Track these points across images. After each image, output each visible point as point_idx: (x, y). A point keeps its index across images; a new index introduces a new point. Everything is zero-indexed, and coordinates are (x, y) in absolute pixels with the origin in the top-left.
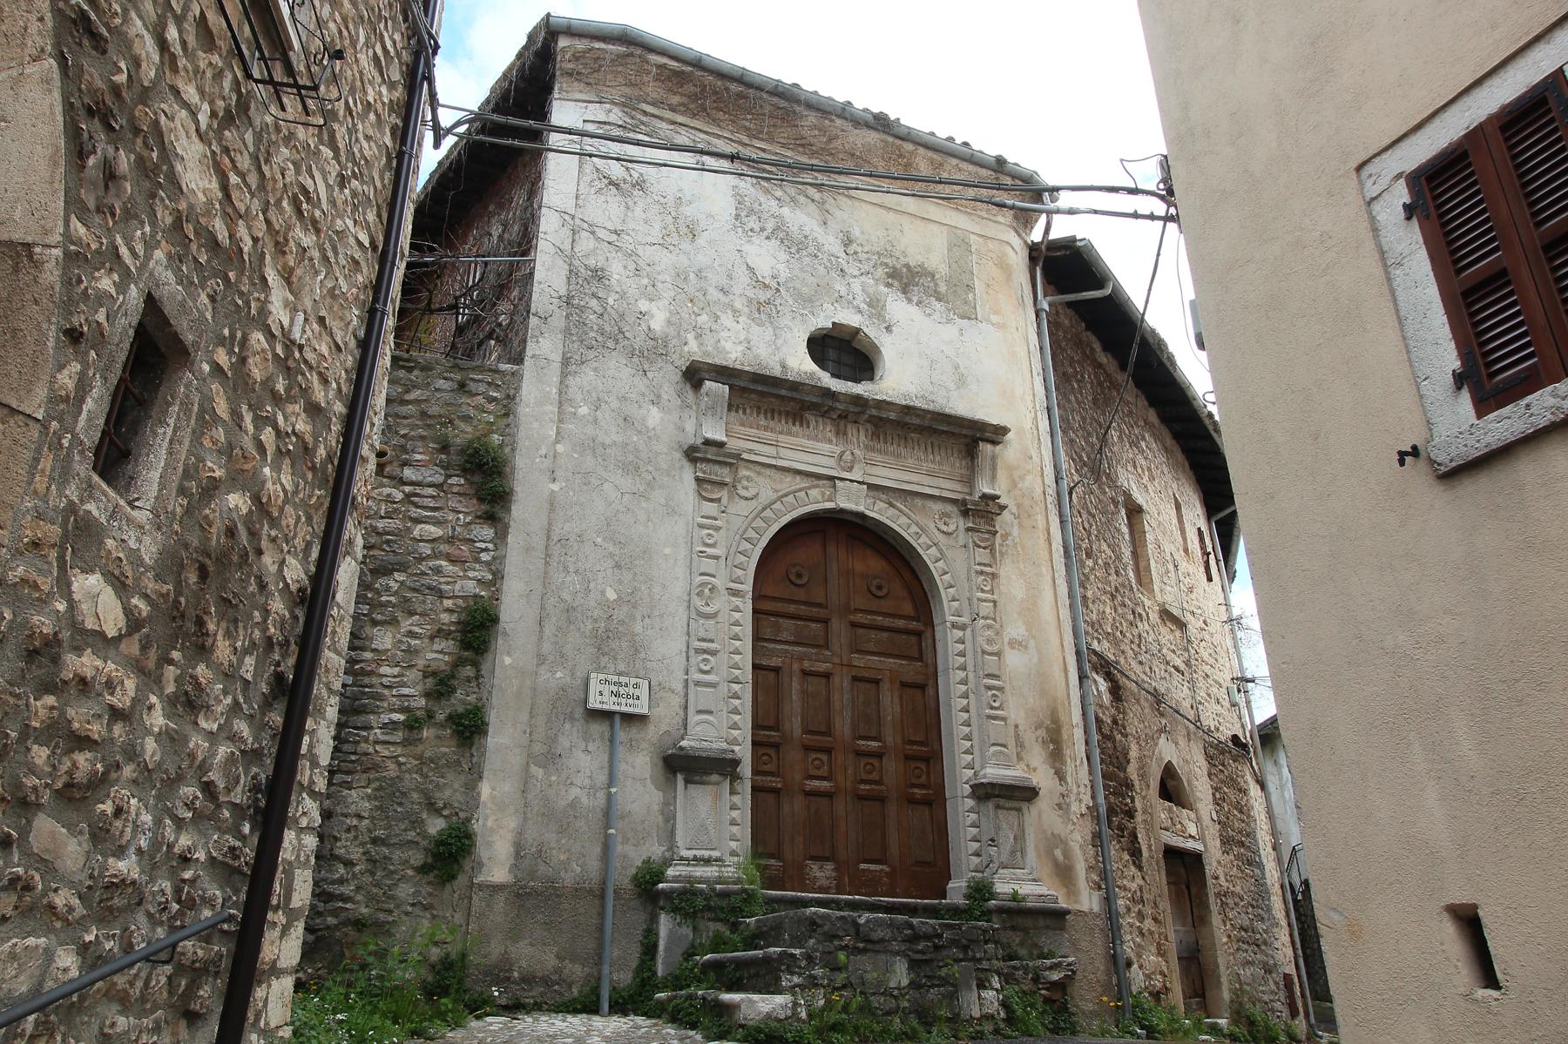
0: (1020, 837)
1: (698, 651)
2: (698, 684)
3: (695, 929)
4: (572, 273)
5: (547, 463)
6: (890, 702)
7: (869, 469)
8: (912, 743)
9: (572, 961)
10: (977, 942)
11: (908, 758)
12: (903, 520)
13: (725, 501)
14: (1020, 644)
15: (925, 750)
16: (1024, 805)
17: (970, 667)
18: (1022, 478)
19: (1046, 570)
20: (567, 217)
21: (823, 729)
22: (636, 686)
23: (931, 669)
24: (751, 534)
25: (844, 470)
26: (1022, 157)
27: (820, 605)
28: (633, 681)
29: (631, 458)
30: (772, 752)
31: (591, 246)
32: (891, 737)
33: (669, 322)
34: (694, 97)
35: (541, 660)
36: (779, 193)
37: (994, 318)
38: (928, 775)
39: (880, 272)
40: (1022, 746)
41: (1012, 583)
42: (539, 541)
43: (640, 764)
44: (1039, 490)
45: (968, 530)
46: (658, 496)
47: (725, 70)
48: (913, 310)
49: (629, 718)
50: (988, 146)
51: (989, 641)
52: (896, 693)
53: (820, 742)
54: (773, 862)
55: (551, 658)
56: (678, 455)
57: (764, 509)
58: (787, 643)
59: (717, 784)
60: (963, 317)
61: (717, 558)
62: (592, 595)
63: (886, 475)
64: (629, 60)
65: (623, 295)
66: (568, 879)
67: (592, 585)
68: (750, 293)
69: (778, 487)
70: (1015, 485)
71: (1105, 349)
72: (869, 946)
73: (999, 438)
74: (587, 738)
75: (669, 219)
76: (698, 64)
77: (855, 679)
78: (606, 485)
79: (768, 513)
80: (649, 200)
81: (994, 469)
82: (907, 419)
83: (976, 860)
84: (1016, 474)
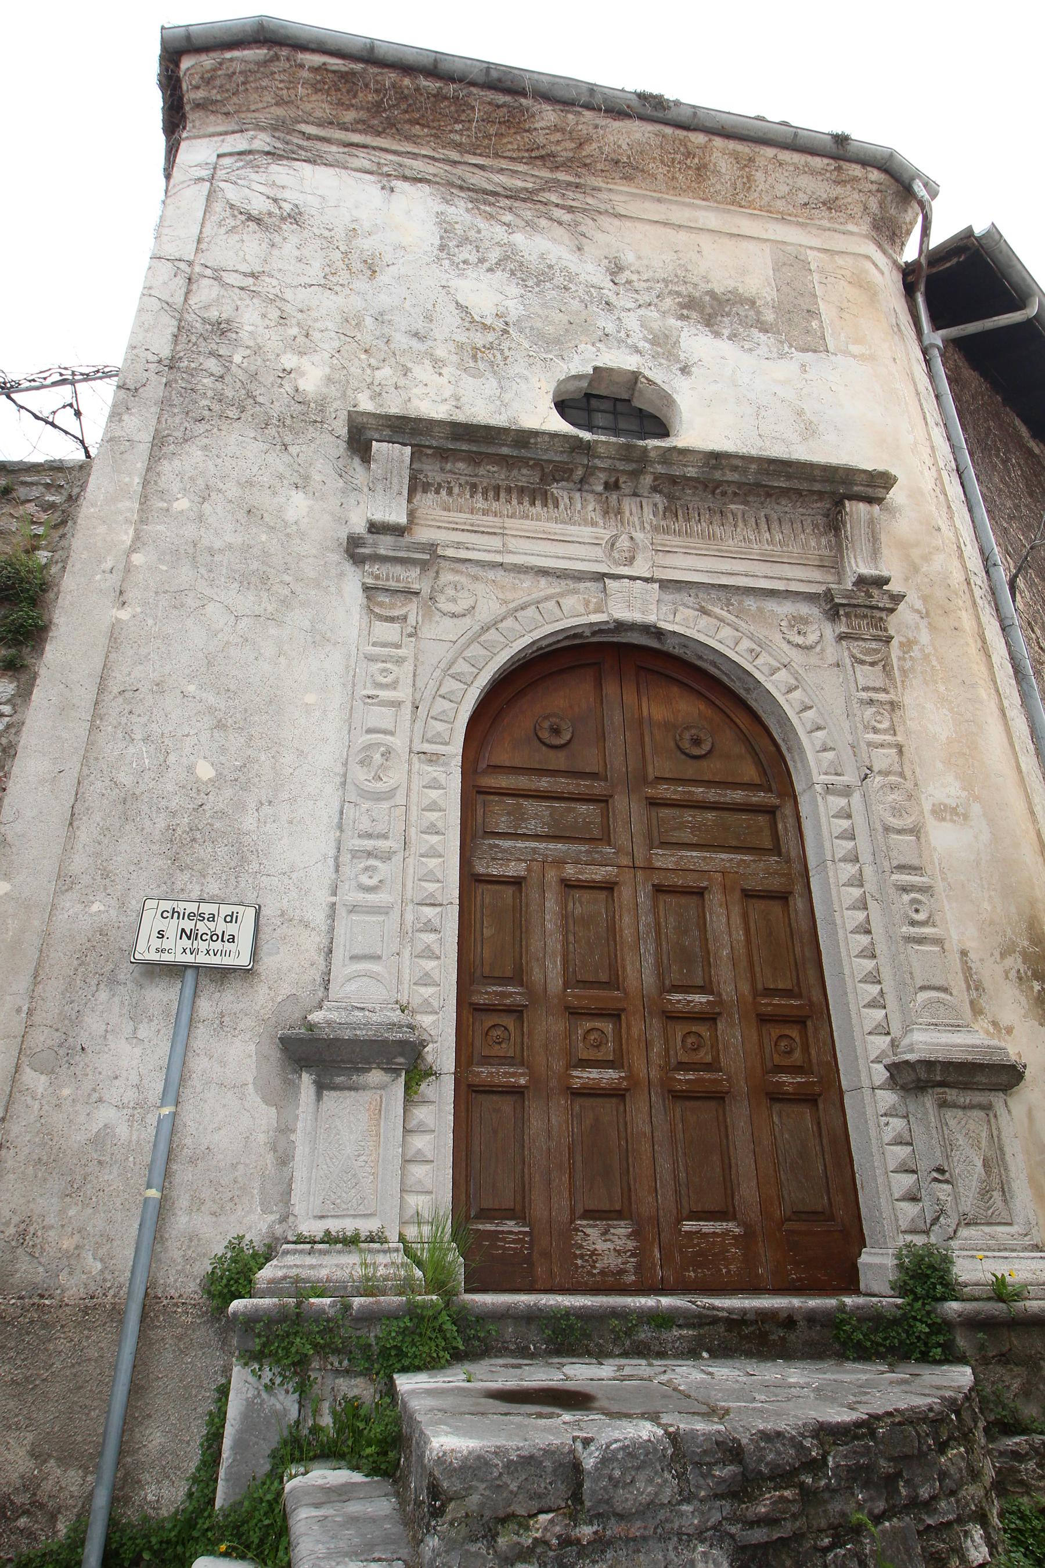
0: (995, 1163)
1: (355, 854)
2: (353, 909)
3: (303, 1390)
4: (182, 329)
5: (114, 580)
6: (724, 924)
7: (661, 559)
8: (769, 992)
9: (62, 1461)
10: (920, 1456)
11: (764, 1019)
12: (726, 632)
13: (412, 620)
14: (954, 811)
15: (795, 1005)
16: (997, 1100)
17: (865, 857)
18: (926, 558)
19: (984, 693)
20: (182, 265)
21: (604, 978)
22: (231, 918)
23: (797, 866)
24: (462, 666)
25: (617, 563)
26: (868, 132)
27: (594, 776)
28: (226, 910)
29: (255, 565)
30: (509, 1021)
31: (214, 293)
32: (730, 983)
33: (329, 380)
34: (377, 108)
35: (65, 881)
36: (508, 217)
37: (854, 349)
38: (806, 1049)
39: (668, 302)
40: (979, 987)
41: (929, 715)
42: (85, 696)
43: (234, 1055)
44: (957, 577)
45: (841, 637)
46: (299, 618)
47: (410, 58)
48: (724, 346)
49: (222, 974)
50: (819, 120)
51: (897, 811)
52: (736, 911)
53: (598, 998)
54: (510, 1225)
55: (86, 880)
56: (336, 557)
57: (485, 629)
58: (536, 837)
59: (383, 1087)
60: (805, 350)
61: (397, 704)
62: (171, 774)
63: (690, 564)
64: (274, 67)
65: (257, 350)
66: (73, 1287)
67: (172, 758)
68: (461, 337)
69: (509, 596)
70: (915, 569)
71: (1034, 436)
72: (614, 1529)
73: (879, 493)
74: (136, 1014)
75: (338, 255)
76: (370, 57)
77: (659, 890)
78: (210, 608)
79: (492, 635)
80: (306, 234)
81: (874, 539)
82: (717, 475)
83: (910, 1210)
84: (915, 553)
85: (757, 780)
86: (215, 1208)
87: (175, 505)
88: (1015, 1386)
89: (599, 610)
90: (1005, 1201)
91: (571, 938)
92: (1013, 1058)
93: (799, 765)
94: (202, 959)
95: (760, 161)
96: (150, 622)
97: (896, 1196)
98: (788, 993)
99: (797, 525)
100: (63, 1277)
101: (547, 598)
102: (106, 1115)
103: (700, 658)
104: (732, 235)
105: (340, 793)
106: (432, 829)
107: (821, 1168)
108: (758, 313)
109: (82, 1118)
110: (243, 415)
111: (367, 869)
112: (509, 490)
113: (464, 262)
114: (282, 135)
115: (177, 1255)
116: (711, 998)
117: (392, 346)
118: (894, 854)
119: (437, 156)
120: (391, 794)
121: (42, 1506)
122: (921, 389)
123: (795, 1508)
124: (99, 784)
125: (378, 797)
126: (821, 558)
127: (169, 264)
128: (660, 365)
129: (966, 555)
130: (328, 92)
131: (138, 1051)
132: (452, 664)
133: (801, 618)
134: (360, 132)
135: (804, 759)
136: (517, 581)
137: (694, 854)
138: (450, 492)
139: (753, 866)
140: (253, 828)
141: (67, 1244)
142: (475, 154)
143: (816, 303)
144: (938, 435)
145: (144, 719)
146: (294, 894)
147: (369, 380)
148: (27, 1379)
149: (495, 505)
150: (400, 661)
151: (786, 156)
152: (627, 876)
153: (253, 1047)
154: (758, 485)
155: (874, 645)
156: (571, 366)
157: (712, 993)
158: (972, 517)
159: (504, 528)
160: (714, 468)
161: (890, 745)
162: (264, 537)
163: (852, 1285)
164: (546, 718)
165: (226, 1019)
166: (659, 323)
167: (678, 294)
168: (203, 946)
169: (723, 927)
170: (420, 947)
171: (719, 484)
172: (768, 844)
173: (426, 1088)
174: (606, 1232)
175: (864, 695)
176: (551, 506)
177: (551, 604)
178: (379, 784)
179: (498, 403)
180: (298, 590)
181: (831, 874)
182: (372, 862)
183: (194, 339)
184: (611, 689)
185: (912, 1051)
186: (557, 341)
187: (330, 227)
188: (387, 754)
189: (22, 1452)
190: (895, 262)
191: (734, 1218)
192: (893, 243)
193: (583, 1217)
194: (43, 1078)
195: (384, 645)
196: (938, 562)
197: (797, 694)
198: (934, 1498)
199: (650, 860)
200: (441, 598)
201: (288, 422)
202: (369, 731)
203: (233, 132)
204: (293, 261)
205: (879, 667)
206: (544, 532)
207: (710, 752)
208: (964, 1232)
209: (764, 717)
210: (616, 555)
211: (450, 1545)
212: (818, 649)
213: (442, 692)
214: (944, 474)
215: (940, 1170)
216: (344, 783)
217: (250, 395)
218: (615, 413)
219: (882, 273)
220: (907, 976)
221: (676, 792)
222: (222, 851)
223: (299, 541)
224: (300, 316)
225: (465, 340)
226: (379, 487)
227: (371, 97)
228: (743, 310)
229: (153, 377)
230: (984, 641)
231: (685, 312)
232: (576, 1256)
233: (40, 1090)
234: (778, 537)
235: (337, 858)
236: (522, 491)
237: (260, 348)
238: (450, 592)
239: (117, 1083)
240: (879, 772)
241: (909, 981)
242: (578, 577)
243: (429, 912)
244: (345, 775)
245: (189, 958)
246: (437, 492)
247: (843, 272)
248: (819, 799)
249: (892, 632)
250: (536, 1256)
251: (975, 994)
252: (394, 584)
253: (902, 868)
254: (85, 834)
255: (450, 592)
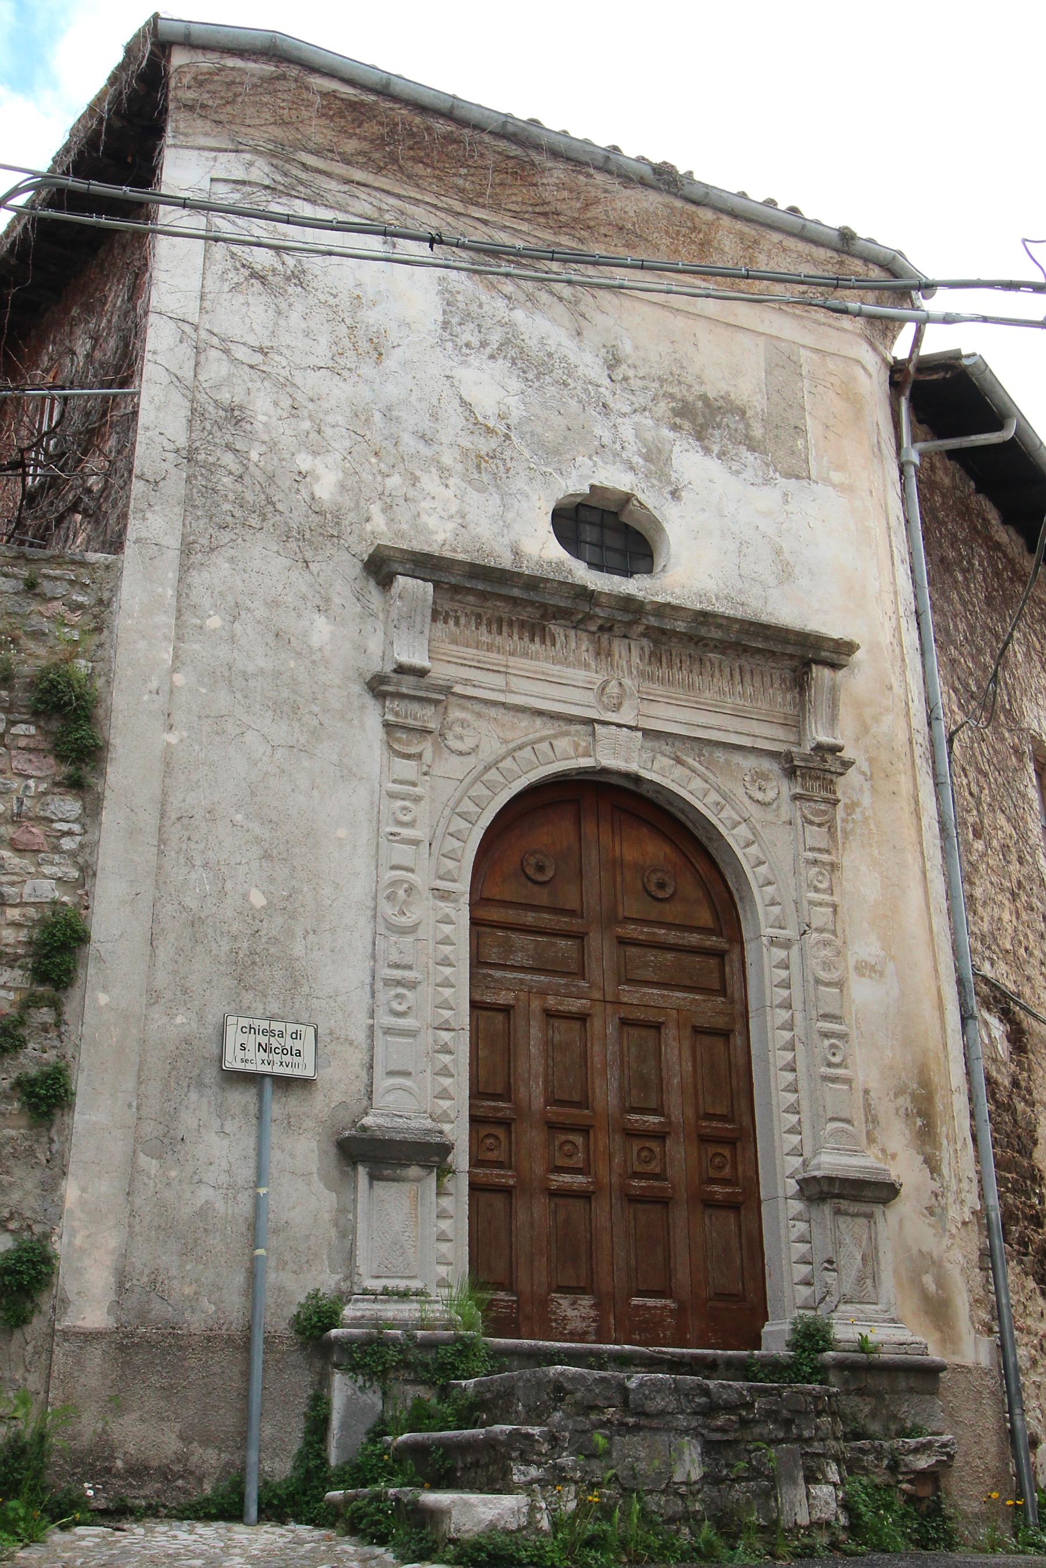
0: (871, 1257)
1: (388, 983)
2: (388, 1031)
4: (196, 414)
6: (676, 1054)
8: (709, 1117)
11: (704, 1139)
12: (697, 784)
13: (428, 757)
14: (872, 968)
15: (729, 1127)
16: (878, 1210)
17: (797, 1005)
18: (876, 719)
20: (187, 328)
21: (576, 1098)
23: (738, 1007)
24: (468, 806)
25: (607, 708)
27: (571, 913)
28: (292, 1028)
29: (286, 693)
30: (500, 1132)
32: (678, 1108)
33: (343, 487)
34: (379, 142)
35: (153, 996)
37: (836, 477)
39: (663, 407)
41: (862, 877)
42: (149, 820)
43: (302, 1151)
44: (902, 737)
45: (796, 797)
47: (426, 99)
48: (713, 466)
49: (285, 1083)
51: (827, 966)
53: (570, 1118)
54: (501, 1295)
55: (168, 995)
56: (357, 688)
57: (487, 769)
59: (418, 1180)
60: (788, 475)
61: (416, 843)
63: (672, 716)
64: (280, 85)
65: (272, 446)
67: (229, 885)
68: (466, 442)
69: (509, 735)
70: (865, 729)
72: (643, 1422)
75: (342, 330)
77: (624, 1022)
78: (249, 736)
79: (493, 775)
81: (834, 705)
82: (703, 631)
83: (804, 1291)
85: (711, 925)
86: (295, 1268)
87: (208, 622)
88: (866, 1410)
89: (587, 754)
90: (874, 1287)
91: (550, 1062)
93: (749, 915)
94: (278, 1070)
95: (765, 245)
96: (197, 747)
97: (796, 1280)
98: (723, 1118)
100: (187, 1315)
101: (541, 740)
102: (205, 1194)
103: (671, 804)
104: (728, 324)
105: (372, 925)
106: (446, 962)
107: (738, 1261)
108: (748, 426)
109: (188, 1195)
110: (264, 524)
111: (397, 996)
112: (511, 624)
114: (280, 163)
115: (270, 1301)
116: (662, 1119)
117: (401, 449)
118: (821, 1004)
119: (440, 205)
120: (413, 929)
121: (192, 1473)
123: (736, 1426)
124: (169, 907)
126: (786, 716)
127: (172, 325)
128: (653, 486)
129: (912, 711)
133: (763, 774)
134: (362, 167)
135: (754, 912)
136: (515, 720)
137: (655, 991)
138: (457, 623)
139: (703, 1005)
140: (302, 954)
142: (477, 204)
143: (804, 418)
144: (903, 573)
147: (380, 489)
148: (171, 1386)
149: (498, 639)
150: (417, 799)
151: (791, 243)
152: (598, 1009)
153: (315, 1144)
155: (823, 807)
156: (570, 482)
157: (662, 1115)
158: (923, 666)
159: (507, 666)
160: (702, 624)
161: (827, 905)
162: (292, 664)
163: (756, 1343)
164: (533, 854)
165: (292, 1120)
166: (653, 433)
167: (672, 396)
168: (277, 1058)
169: (675, 1059)
170: (439, 1066)
171: (703, 638)
172: (716, 986)
173: (449, 1184)
174: (574, 1303)
175: (810, 855)
176: (548, 643)
177: (544, 746)
178: (403, 919)
179: (501, 523)
180: (326, 722)
181: (769, 1018)
182: (400, 990)
183: (208, 427)
184: (589, 828)
185: (819, 1169)
187: (334, 292)
189: (174, 1436)
190: (884, 360)
192: (885, 336)
193: (556, 1292)
194: (154, 1161)
195: (402, 782)
196: (888, 719)
197: (753, 850)
198: (811, 1438)
199: (618, 995)
200: (450, 736)
201: (307, 536)
202: (394, 868)
203: (226, 151)
204: (300, 336)
205: (825, 829)
206: (543, 673)
207: (672, 895)
208: (842, 1307)
209: (721, 865)
210: (605, 699)
212: (774, 806)
213: (451, 830)
214: (903, 621)
216: (375, 917)
217: (270, 502)
218: (602, 526)
219: (870, 376)
220: (821, 1109)
221: (642, 932)
222: (278, 974)
223: (323, 669)
224: (311, 406)
225: (469, 445)
226: (404, 625)
228: (732, 421)
229: (173, 471)
230: (917, 802)
231: (678, 420)
232: (551, 1320)
233: (153, 1172)
234: (749, 690)
235: (372, 985)
236: (522, 625)
237: (275, 444)
238: (458, 729)
239: (212, 1168)
240: (816, 929)
241: (822, 1113)
242: (570, 719)
243: (446, 1036)
244: (375, 908)
245: (266, 1069)
246: (446, 622)
247: (833, 379)
248: (765, 950)
249: (839, 795)
250: (521, 1319)
251: (871, 1126)
252: (412, 722)
253: (825, 1017)
254: (164, 954)
255: (458, 729)
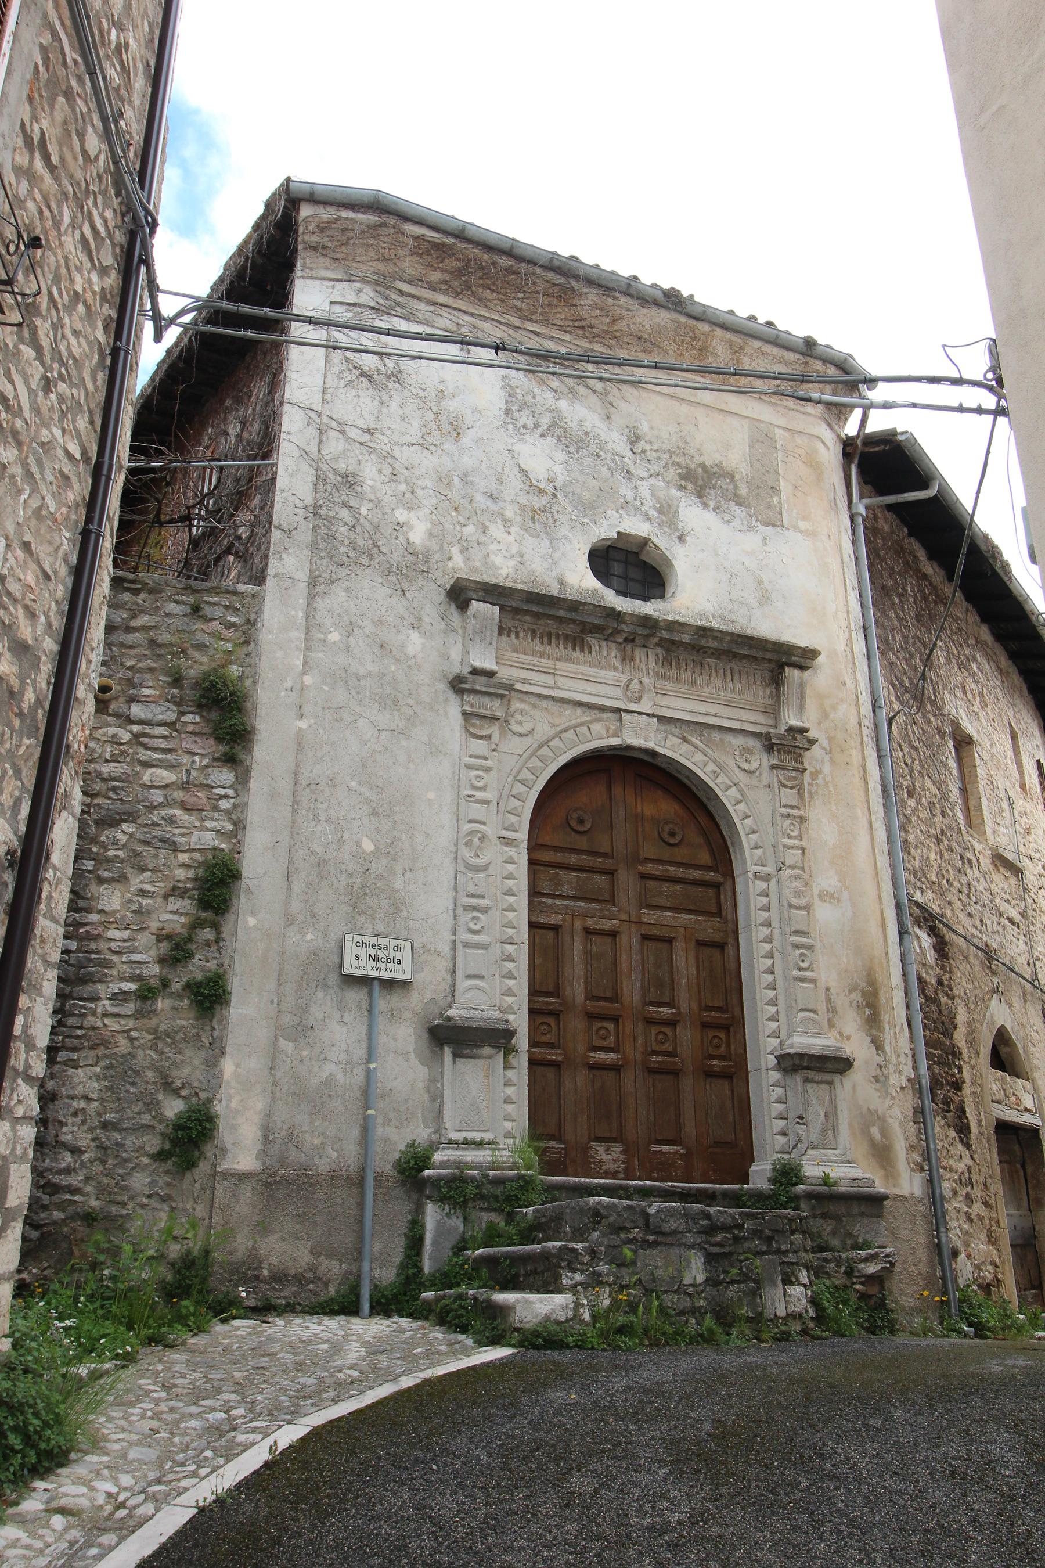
0: (831, 1115)
1: (467, 908)
2: (467, 945)
4: (320, 479)
6: (684, 962)
7: (661, 700)
9: (328, 1257)
11: (705, 1026)
12: (699, 757)
14: (832, 896)
15: (724, 1016)
16: (837, 1078)
17: (775, 923)
18: (834, 708)
20: (313, 415)
21: (609, 994)
23: (731, 925)
24: (526, 775)
25: (630, 700)
26: (831, 337)
27: (604, 855)
28: (394, 943)
29: (388, 690)
30: (551, 1020)
32: (686, 1002)
33: (430, 534)
34: (457, 274)
35: (290, 920)
37: (803, 525)
39: (672, 473)
40: (834, 1011)
41: (824, 827)
42: (285, 786)
43: (402, 1036)
44: (853, 721)
45: (773, 767)
47: (492, 241)
48: (710, 518)
49: (389, 985)
51: (797, 894)
53: (604, 1010)
55: (301, 918)
56: (442, 686)
57: (540, 746)
58: (568, 897)
59: (490, 1057)
60: (767, 524)
61: (487, 802)
62: (346, 847)
63: (680, 707)
64: (382, 231)
65: (377, 504)
67: (346, 835)
68: (523, 500)
69: (557, 721)
70: (826, 715)
72: (660, 1239)
73: (808, 663)
74: (342, 1006)
75: (430, 416)
77: (645, 937)
78: (361, 723)
79: (545, 751)
80: (406, 393)
81: (802, 697)
82: (703, 642)
83: (782, 1140)
87: (330, 636)
88: (829, 1229)
89: (616, 735)
92: (848, 1054)
95: (748, 350)
98: (719, 1009)
99: (751, 678)
102: (329, 1068)
104: (721, 410)
108: (736, 487)
109: (316, 1069)
112: (558, 637)
113: (524, 427)
115: (379, 1149)
118: (793, 923)
120: (484, 868)
121: (320, 1279)
122: (846, 559)
124: (301, 852)
125: (478, 869)
127: (301, 412)
130: (421, 256)
131: (345, 1029)
132: (518, 773)
138: (517, 637)
141: (316, 1141)
142: (531, 320)
145: (325, 806)
146: (430, 933)
154: (729, 651)
155: (794, 774)
156: (602, 530)
160: (702, 636)
161: (797, 848)
162: (393, 668)
164: (575, 810)
167: (679, 465)
168: (383, 966)
170: (505, 971)
171: (703, 647)
173: (513, 1060)
175: (784, 810)
178: (478, 860)
182: (475, 914)
184: (617, 790)
186: (592, 507)
188: (482, 839)
190: (838, 436)
191: (680, 1144)
195: (476, 757)
196: (843, 707)
198: (787, 1251)
200: (512, 721)
202: (470, 821)
205: (795, 791)
208: (810, 1152)
210: (629, 693)
211: (603, 1235)
213: (514, 793)
215: (801, 1117)
216: (456, 858)
217: (375, 545)
218: (626, 563)
224: (406, 473)
225: (525, 502)
227: (455, 264)
229: (303, 522)
230: (865, 770)
231: (683, 483)
234: (738, 686)
235: (454, 910)
236: (566, 637)
238: (518, 717)
242: (603, 709)
243: (510, 948)
245: (374, 974)
253: (796, 932)
254: (298, 887)
255: (518, 717)
